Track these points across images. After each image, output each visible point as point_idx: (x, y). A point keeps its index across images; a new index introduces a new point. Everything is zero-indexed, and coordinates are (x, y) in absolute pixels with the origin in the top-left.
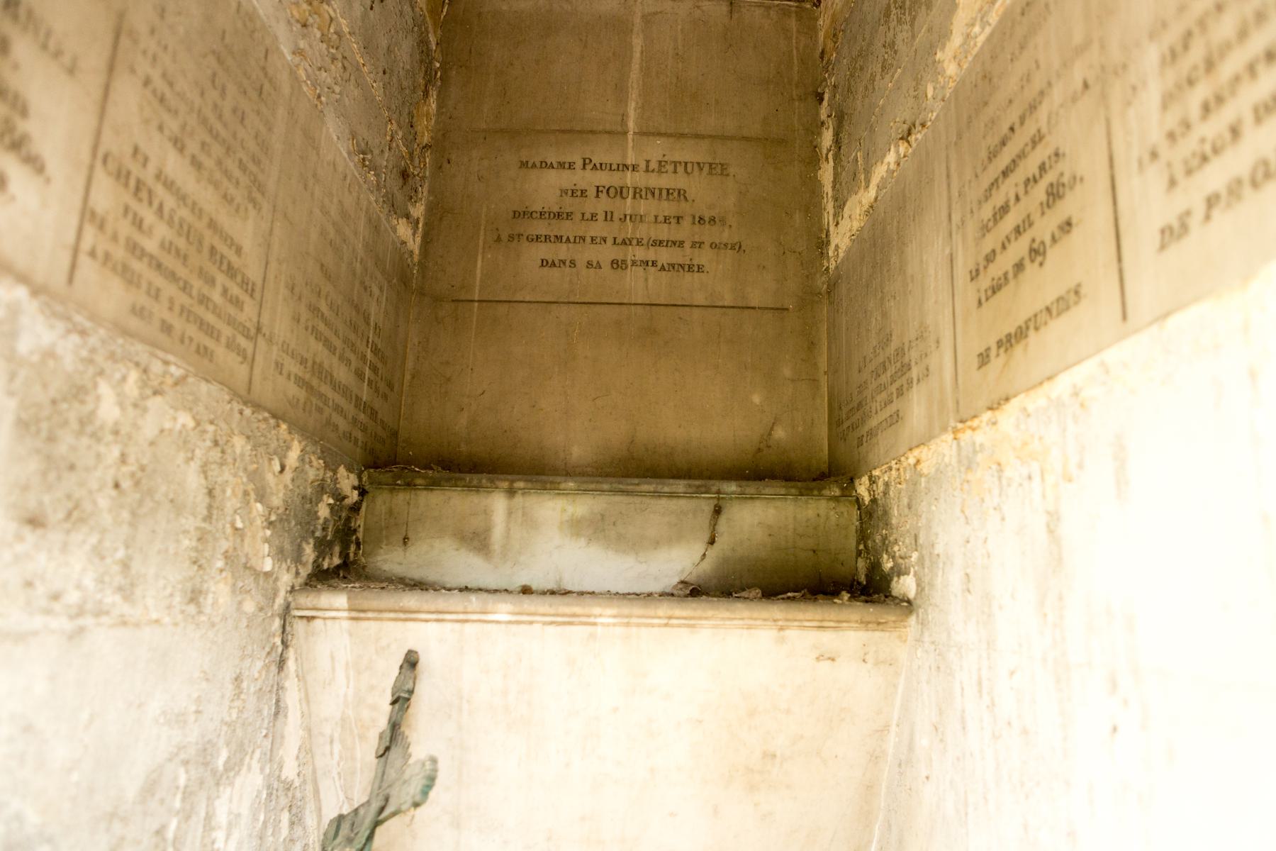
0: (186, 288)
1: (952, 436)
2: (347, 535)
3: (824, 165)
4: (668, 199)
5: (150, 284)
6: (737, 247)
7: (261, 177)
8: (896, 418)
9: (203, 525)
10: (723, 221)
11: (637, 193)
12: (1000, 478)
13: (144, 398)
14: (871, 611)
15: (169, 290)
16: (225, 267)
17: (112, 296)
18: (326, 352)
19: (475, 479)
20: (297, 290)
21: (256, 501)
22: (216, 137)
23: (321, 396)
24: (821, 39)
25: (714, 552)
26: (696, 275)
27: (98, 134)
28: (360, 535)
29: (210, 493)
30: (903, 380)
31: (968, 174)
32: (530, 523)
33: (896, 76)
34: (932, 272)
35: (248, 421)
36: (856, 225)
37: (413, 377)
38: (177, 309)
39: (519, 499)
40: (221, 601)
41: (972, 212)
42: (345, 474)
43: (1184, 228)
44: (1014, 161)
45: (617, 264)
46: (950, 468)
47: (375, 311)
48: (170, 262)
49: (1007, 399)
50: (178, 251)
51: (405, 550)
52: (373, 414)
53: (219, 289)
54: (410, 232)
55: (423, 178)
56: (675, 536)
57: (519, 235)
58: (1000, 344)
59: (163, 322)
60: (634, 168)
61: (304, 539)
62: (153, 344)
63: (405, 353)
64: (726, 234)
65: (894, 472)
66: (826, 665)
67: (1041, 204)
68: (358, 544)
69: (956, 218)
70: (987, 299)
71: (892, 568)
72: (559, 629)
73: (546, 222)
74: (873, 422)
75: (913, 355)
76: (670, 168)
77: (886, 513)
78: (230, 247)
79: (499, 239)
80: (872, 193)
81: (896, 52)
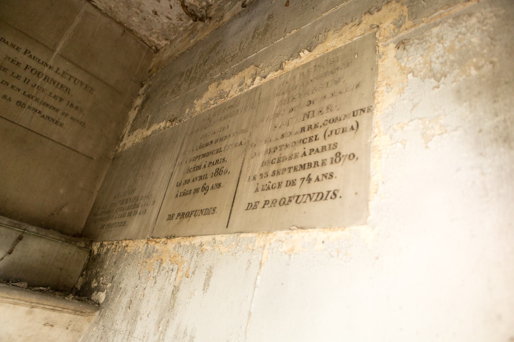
1: (146, 241)
3: (132, 110)
4: (60, 89)
6: (83, 124)
8: (124, 224)
10: (81, 111)
11: (46, 78)
14: (81, 306)
24: (152, 66)
25: (8, 258)
26: (58, 127)
30: (133, 211)
33: (176, 98)
36: (137, 140)
43: (255, 207)
45: (19, 103)
49: (174, 237)
58: (179, 214)
60: (50, 67)
65: (114, 246)
66: (48, 328)
69: (179, 160)
71: (96, 287)
74: (112, 221)
75: (142, 202)
76: (68, 77)
77: (103, 262)
80: (149, 133)
81: (179, 90)
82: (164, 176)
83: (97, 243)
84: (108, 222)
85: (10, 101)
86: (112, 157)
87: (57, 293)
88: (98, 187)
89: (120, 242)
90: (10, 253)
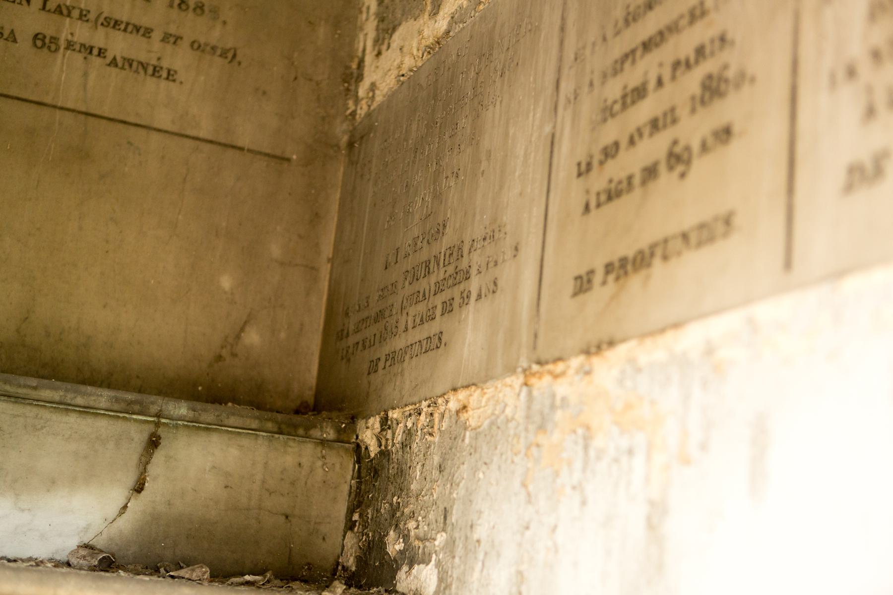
1: (521, 379)
6: (230, 56)
8: (437, 343)
10: (215, 12)
12: (586, 448)
25: (138, 505)
26: (163, 84)
30: (456, 292)
31: (593, 34)
34: (520, 151)
36: (408, 62)
41: (591, 84)
44: (661, 33)
45: (41, 41)
46: (512, 425)
49: (611, 343)
56: (85, 475)
58: (609, 268)
64: (217, 33)
65: (423, 417)
67: (693, 98)
69: (567, 87)
70: (599, 205)
74: (399, 343)
77: (401, 472)
80: (442, 24)
82: (526, 155)
83: (371, 421)
84: (387, 349)
85: (15, 41)
86: (345, 138)
87: (296, 585)
88: (327, 250)
89: (440, 401)
90: (139, 488)
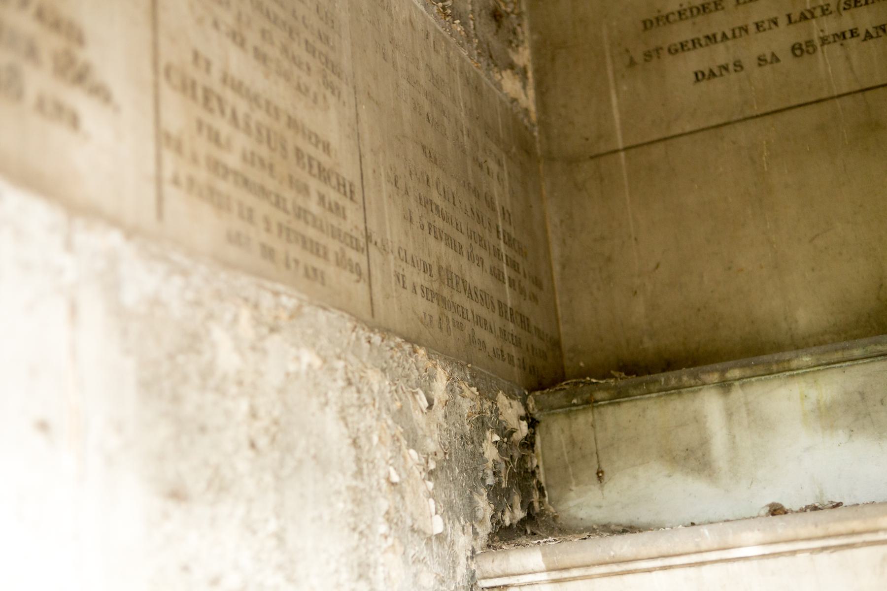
0: (279, 202)
2: (525, 479)
5: (240, 204)
7: (332, 56)
9: (354, 483)
13: (262, 338)
15: (263, 208)
16: (315, 170)
17: (203, 225)
18: (451, 252)
19: (672, 377)
20: (401, 183)
21: (408, 447)
22: (275, 21)
23: (457, 308)
27: (155, 46)
28: (542, 479)
29: (355, 443)
32: (762, 424)
35: (380, 350)
37: (564, 267)
38: (274, 228)
39: (737, 394)
40: (394, 575)
42: (506, 402)
45: (798, 50)
47: (499, 193)
48: (256, 175)
50: (262, 161)
51: (602, 488)
52: (524, 322)
53: (314, 197)
54: (518, 85)
55: (520, 15)
57: (658, 50)
59: (263, 247)
61: (474, 489)
62: (259, 274)
63: (547, 241)
68: (541, 490)
72: (836, 556)
73: (690, 21)
78: (316, 146)
79: (632, 63)
